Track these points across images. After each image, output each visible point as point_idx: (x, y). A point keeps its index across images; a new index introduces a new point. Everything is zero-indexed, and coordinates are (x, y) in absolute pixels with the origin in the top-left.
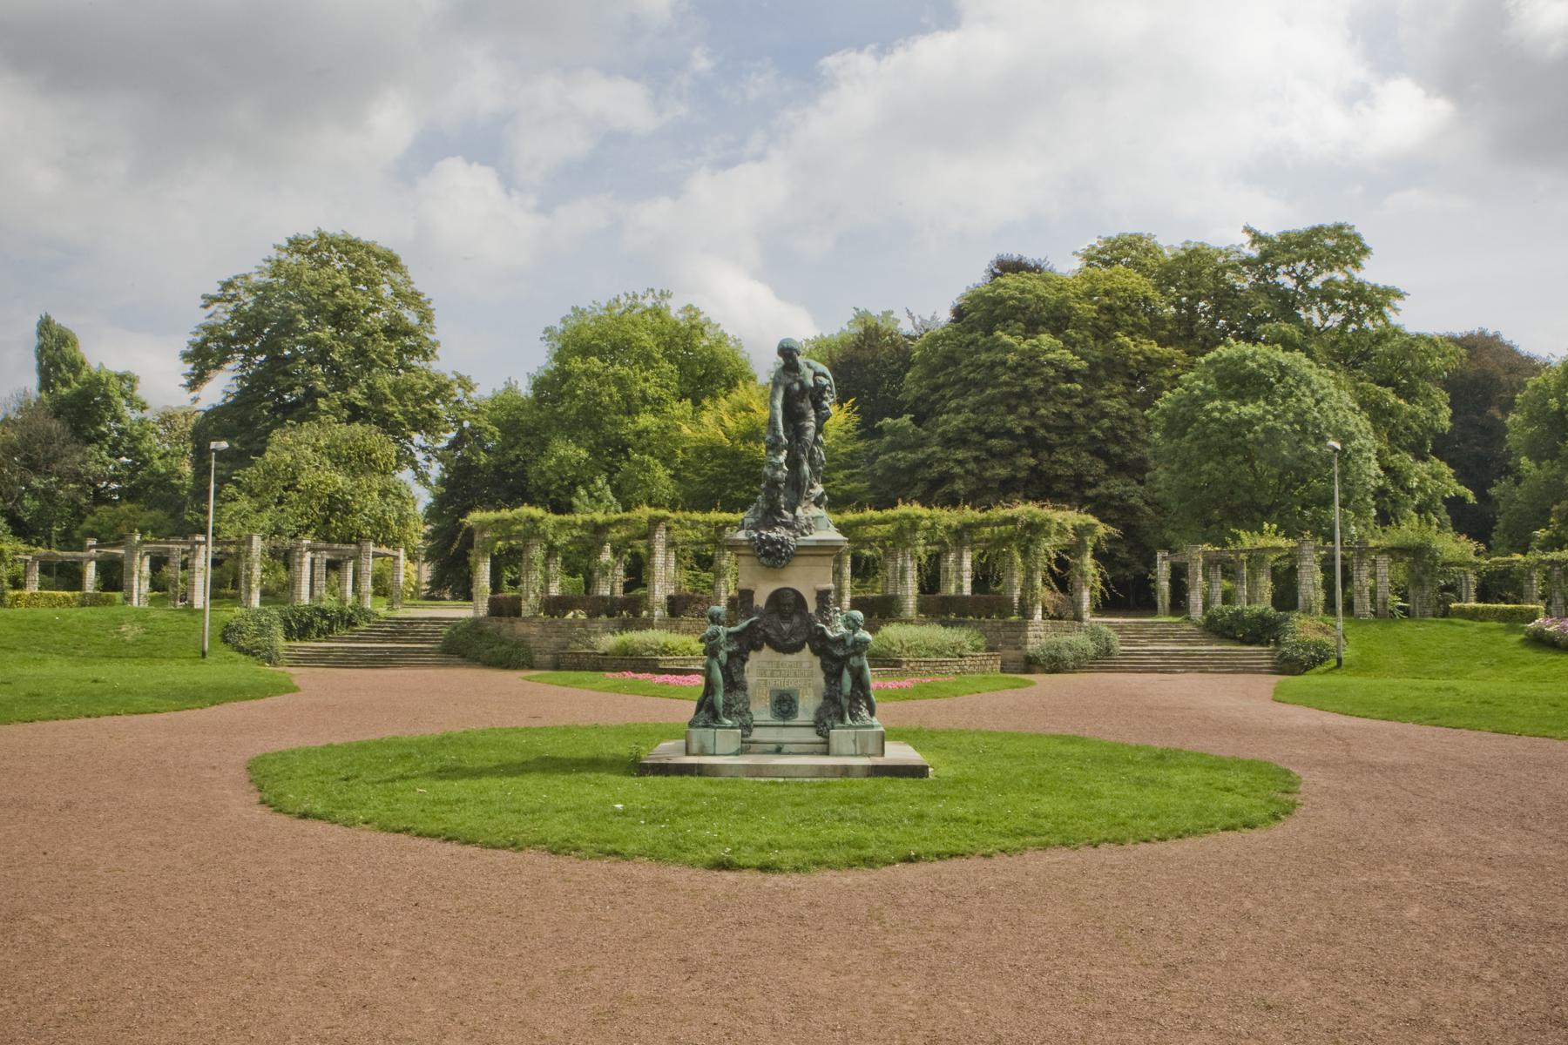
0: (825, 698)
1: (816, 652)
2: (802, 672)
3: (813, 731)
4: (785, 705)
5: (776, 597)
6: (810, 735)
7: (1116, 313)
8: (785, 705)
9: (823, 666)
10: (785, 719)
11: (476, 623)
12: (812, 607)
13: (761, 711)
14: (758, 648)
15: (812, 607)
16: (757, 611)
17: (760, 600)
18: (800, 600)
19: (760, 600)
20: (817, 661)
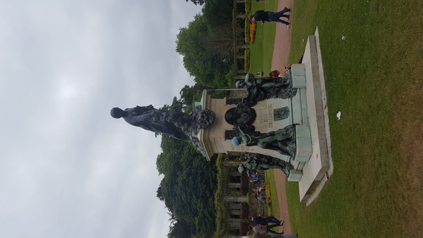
0: (277, 97)
1: (255, 103)
2: (265, 108)
3: (293, 98)
4: (281, 114)
5: (229, 121)
6: (296, 99)
7: (178, 167)
8: (281, 114)
9: (262, 99)
10: (288, 111)
11: (216, 164)
12: (234, 106)
13: (285, 123)
14: (254, 128)
15: (234, 106)
16: (236, 129)
17: (230, 127)
18: (230, 111)
19: (230, 127)
20: (260, 103)
